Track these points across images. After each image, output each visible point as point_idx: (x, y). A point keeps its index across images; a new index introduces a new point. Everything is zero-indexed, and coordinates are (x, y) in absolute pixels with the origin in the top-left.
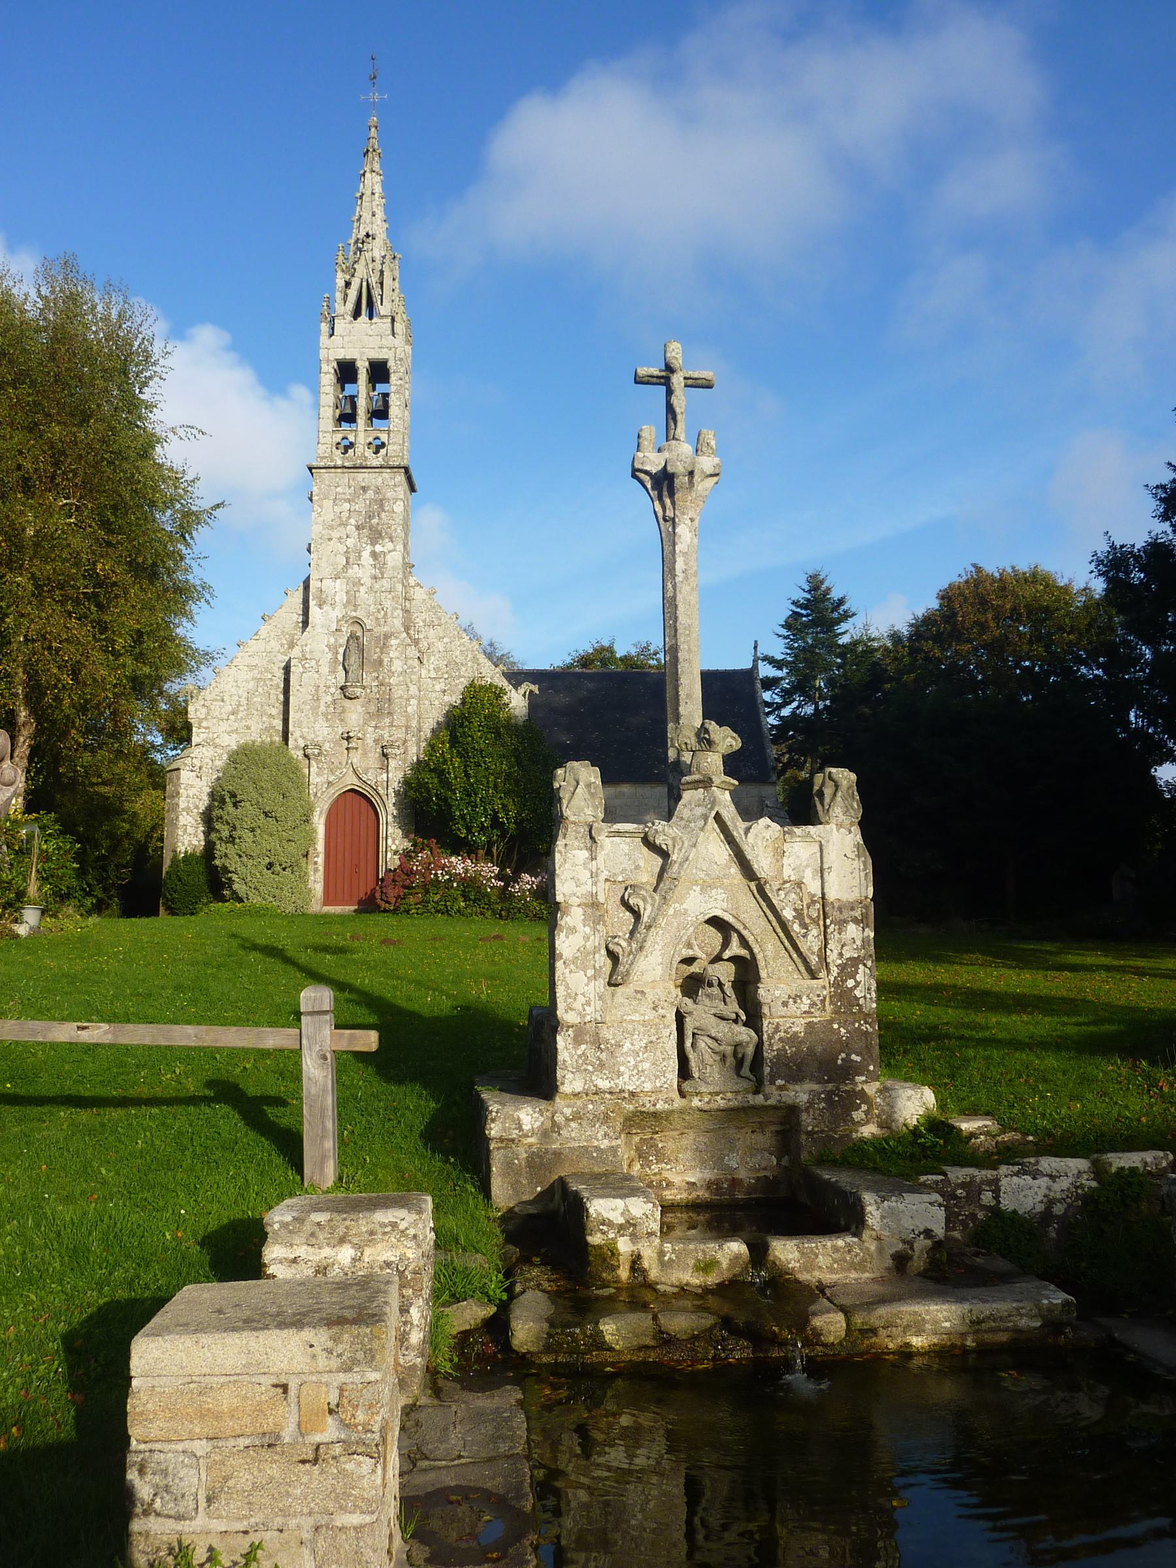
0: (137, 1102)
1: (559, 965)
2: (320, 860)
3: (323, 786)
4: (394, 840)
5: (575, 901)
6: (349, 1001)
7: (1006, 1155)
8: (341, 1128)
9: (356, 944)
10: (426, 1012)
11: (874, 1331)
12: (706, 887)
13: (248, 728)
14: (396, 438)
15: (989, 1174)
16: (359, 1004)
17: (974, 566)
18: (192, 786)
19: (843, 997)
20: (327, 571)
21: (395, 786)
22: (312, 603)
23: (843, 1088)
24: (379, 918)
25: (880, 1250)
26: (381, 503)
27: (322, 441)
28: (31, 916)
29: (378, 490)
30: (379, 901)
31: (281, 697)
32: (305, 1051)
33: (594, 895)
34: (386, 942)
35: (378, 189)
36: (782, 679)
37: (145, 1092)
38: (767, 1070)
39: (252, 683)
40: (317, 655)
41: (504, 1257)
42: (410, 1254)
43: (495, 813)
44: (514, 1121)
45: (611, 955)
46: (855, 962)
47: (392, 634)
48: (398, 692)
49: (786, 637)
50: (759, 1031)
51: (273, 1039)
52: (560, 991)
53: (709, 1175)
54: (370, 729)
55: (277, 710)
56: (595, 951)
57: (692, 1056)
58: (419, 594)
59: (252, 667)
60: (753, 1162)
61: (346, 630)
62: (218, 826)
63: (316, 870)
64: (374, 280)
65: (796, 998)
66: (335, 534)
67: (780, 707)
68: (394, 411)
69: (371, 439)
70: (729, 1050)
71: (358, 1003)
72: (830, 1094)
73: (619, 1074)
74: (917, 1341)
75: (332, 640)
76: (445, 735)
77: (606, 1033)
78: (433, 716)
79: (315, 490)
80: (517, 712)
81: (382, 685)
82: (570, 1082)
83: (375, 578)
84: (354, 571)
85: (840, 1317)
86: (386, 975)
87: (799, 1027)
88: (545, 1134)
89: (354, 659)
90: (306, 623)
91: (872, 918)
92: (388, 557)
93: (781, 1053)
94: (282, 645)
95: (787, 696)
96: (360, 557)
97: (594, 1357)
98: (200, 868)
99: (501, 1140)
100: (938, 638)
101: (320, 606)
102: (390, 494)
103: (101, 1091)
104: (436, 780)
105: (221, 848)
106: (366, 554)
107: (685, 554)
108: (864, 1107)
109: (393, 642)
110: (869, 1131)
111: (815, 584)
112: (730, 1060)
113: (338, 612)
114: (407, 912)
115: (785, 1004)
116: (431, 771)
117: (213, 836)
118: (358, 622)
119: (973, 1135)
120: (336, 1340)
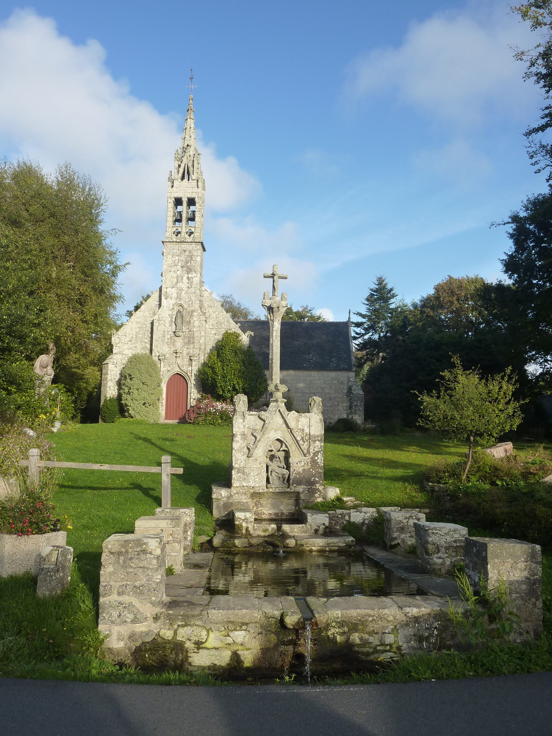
0: (111, 489)
1: (233, 451)
2: (164, 401)
3: (166, 372)
4: (194, 394)
5: (239, 433)
6: (174, 459)
7: (355, 507)
8: (172, 496)
9: (178, 437)
10: (200, 463)
11: (303, 545)
12: (276, 430)
13: (136, 347)
14: (198, 230)
15: (348, 511)
16: (178, 460)
17: (449, 276)
18: (113, 370)
19: (314, 462)
20: (169, 284)
21: (195, 372)
22: (163, 297)
23: (313, 487)
24: (187, 426)
25: (311, 528)
26: (191, 257)
27: (168, 231)
28: (57, 424)
29: (190, 252)
30: (187, 419)
31: (150, 335)
32: (163, 473)
33: (244, 432)
34: (189, 437)
35: (192, 126)
36: (365, 323)
37: (112, 486)
38: (291, 482)
39: (138, 329)
40: (164, 319)
41: (215, 528)
42: (188, 519)
43: (234, 385)
44: (220, 494)
45: (248, 448)
46: (318, 452)
47: (195, 311)
48: (196, 334)
49: (367, 305)
50: (289, 471)
51: (154, 469)
52: (234, 458)
53: (275, 511)
54: (185, 349)
55: (148, 340)
56: (244, 447)
57: (270, 477)
58: (206, 294)
59: (138, 323)
60: (288, 508)
61: (176, 309)
62: (123, 387)
63: (162, 406)
64: (190, 165)
65: (300, 462)
66: (173, 269)
67: (364, 335)
68: (197, 219)
69: (187, 230)
70: (281, 476)
71: (178, 460)
72: (309, 489)
73: (249, 482)
74: (314, 548)
75: (171, 313)
76: (215, 352)
77: (246, 470)
78: (211, 345)
79: (165, 251)
80: (245, 343)
81: (190, 331)
82: (235, 483)
83: (188, 287)
84: (180, 285)
85: (294, 541)
86: (188, 450)
87: (301, 470)
88: (228, 498)
89: (179, 320)
90: (160, 305)
91: (323, 440)
92: (194, 279)
93: (295, 477)
94: (150, 314)
95: (367, 330)
96: (182, 279)
97: (233, 549)
98: (116, 404)
99: (216, 499)
100: (433, 308)
101: (166, 299)
102: (195, 253)
103: (97, 485)
104: (211, 371)
105: (124, 396)
106: (185, 278)
107: (276, 331)
108: (319, 493)
109: (195, 314)
110: (320, 500)
111: (380, 281)
112: (281, 479)
113: (173, 301)
114: (198, 424)
115: (297, 464)
116: (209, 367)
117: (122, 391)
118: (181, 305)
119: (347, 501)
120: (172, 522)
